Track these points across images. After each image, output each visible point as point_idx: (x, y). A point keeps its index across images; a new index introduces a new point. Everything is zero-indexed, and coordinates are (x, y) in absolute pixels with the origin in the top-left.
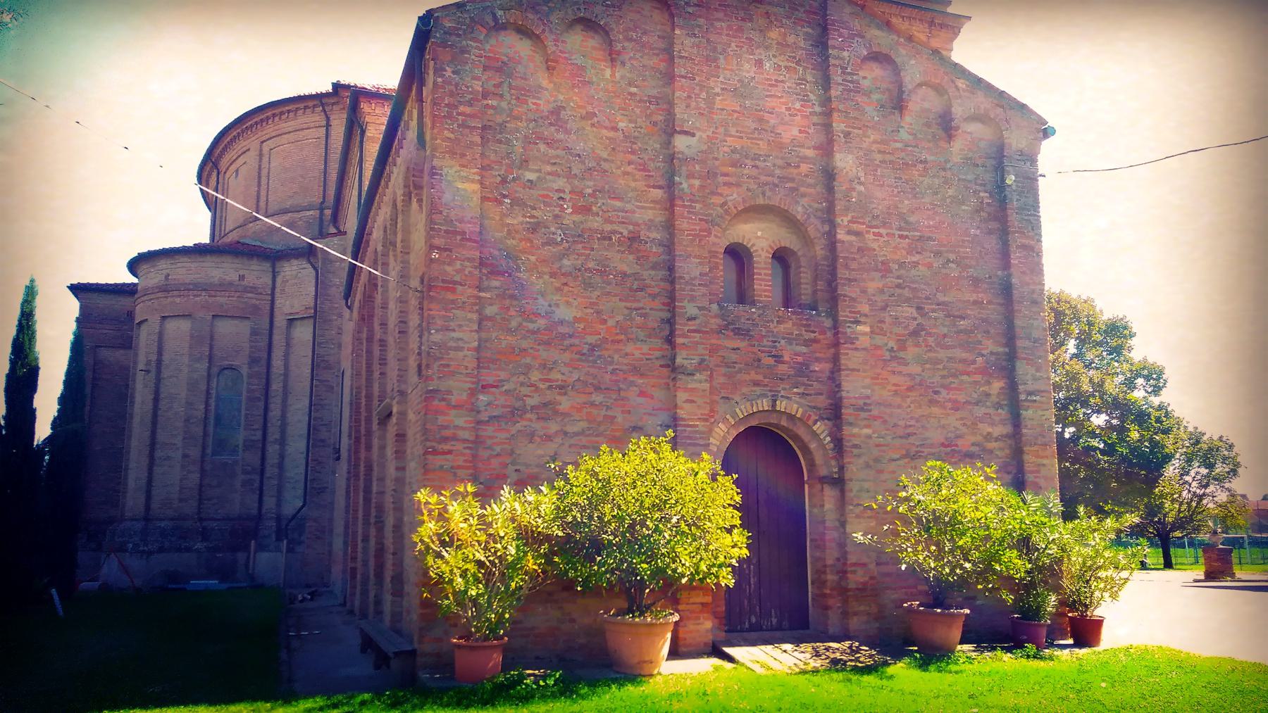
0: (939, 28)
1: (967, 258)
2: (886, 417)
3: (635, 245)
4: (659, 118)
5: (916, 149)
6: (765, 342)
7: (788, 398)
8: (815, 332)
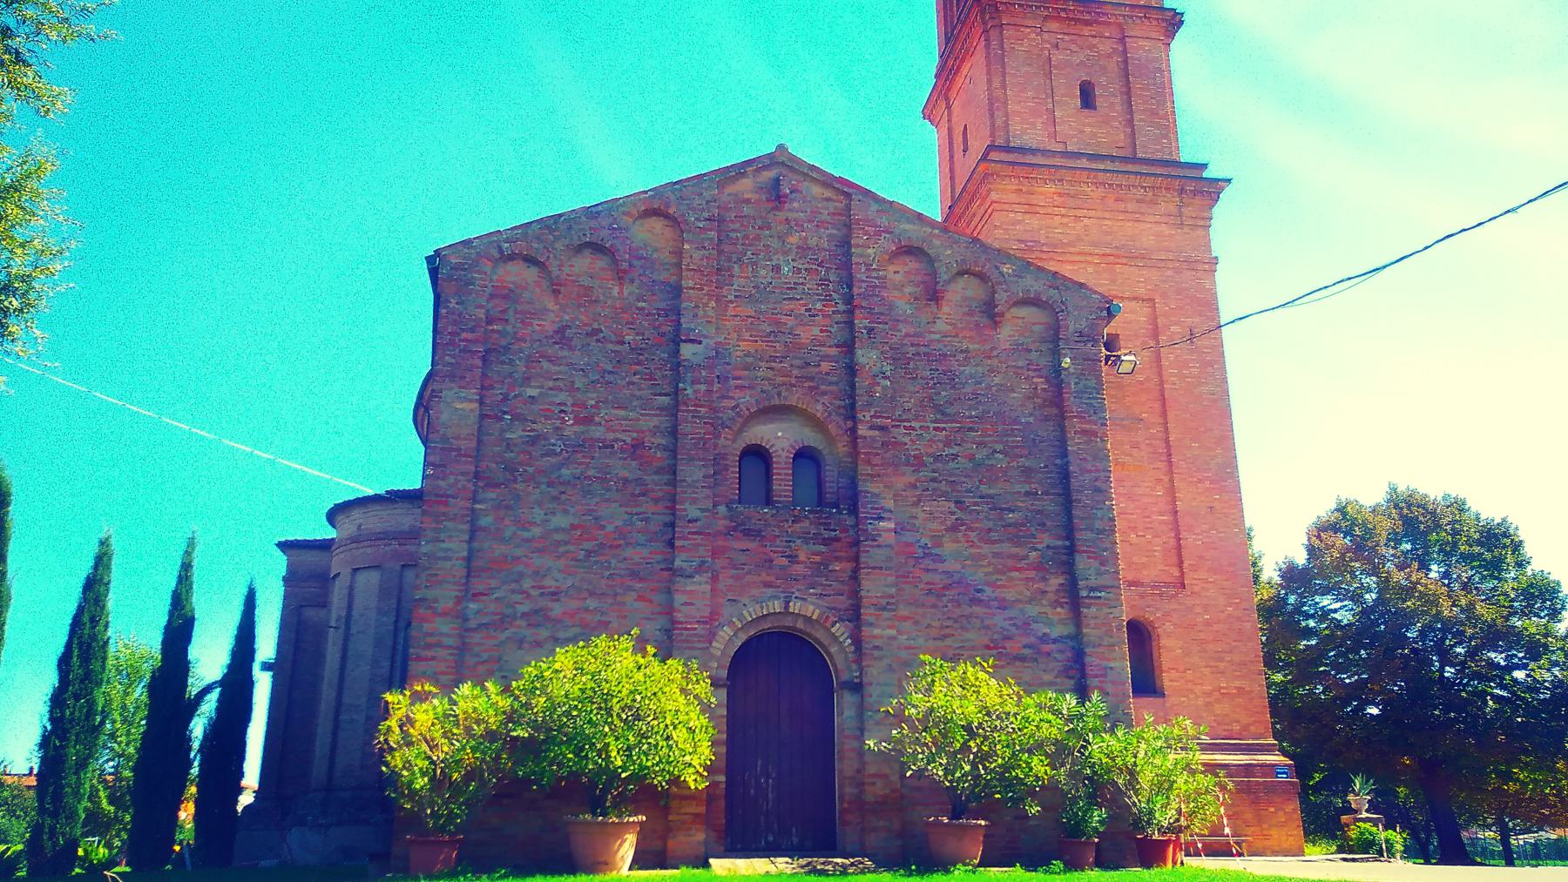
0: (1191, 195)
1: (1017, 447)
2: (917, 617)
3: (639, 452)
4: (667, 329)
5: (956, 339)
6: (778, 542)
7: (803, 599)
8: (835, 531)
